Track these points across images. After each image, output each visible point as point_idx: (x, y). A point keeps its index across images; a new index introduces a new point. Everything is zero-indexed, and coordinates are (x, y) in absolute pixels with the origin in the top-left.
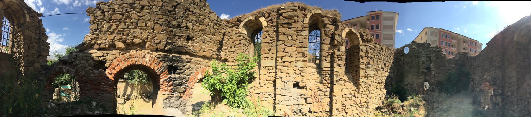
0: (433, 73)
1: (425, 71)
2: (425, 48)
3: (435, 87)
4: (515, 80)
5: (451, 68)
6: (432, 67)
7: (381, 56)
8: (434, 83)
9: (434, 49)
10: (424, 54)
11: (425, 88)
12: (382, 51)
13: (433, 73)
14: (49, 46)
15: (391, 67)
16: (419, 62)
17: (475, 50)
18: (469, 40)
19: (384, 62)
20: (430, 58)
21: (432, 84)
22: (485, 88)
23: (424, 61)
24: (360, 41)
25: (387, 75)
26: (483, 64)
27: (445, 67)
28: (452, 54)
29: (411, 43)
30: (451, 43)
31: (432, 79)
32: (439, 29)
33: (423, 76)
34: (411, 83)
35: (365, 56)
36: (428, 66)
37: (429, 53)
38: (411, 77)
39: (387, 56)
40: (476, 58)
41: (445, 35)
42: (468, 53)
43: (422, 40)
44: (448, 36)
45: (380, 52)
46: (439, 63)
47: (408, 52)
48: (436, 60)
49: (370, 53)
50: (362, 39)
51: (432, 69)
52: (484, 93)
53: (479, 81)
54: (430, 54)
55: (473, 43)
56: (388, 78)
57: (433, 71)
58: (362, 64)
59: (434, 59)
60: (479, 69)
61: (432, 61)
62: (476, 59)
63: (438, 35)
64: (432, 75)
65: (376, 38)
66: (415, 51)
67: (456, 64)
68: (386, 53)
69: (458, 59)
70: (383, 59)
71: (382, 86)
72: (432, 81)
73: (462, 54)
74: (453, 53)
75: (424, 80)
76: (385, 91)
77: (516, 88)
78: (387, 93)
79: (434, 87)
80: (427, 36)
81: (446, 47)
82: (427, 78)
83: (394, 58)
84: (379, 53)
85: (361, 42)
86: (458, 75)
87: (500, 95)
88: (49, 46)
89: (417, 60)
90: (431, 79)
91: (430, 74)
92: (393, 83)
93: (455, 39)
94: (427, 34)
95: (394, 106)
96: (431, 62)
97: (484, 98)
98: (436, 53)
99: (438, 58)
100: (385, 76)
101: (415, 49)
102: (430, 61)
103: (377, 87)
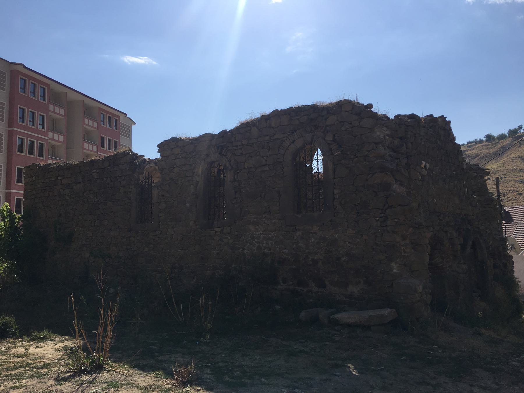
14: (452, 131)
17: (116, 142)
18: (100, 109)
32: (11, 63)
41: (29, 88)
44: (39, 92)
55: (109, 118)
81: (24, 128)
88: (452, 131)
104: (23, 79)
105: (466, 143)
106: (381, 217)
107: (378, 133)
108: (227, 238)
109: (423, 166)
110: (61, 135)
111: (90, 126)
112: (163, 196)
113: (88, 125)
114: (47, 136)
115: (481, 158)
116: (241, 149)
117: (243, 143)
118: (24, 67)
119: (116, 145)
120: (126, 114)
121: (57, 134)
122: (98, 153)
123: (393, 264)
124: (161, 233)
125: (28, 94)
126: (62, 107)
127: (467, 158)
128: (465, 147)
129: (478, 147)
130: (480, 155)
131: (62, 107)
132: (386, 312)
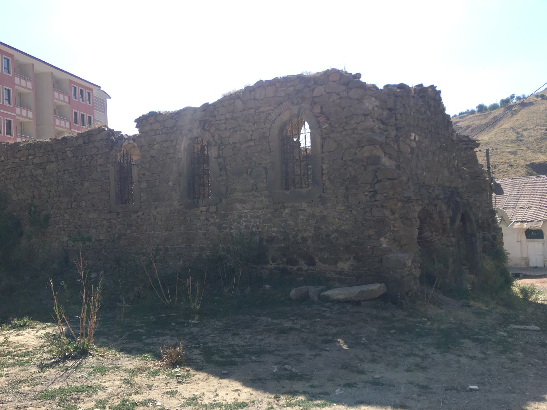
17: (90, 118)
18: (71, 82)
65: (7, 134)
105: (458, 114)
106: (370, 192)
107: (367, 105)
108: (214, 217)
109: (412, 138)
112: (144, 174)
113: (59, 99)
115: (473, 129)
116: (225, 123)
117: (227, 116)
120: (100, 87)
121: (26, 110)
122: (71, 130)
123: (382, 239)
124: (143, 214)
127: (459, 130)
128: (457, 118)
129: (470, 118)
130: (472, 126)
132: (375, 287)
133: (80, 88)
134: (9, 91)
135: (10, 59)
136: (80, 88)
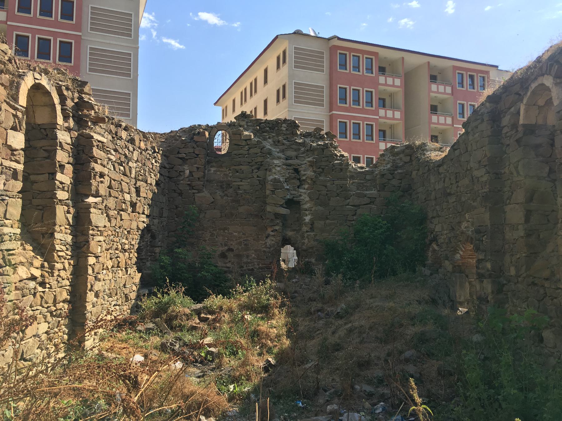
0: (307, 219)
1: (284, 211)
2: (280, 138)
3: (316, 260)
4: (522, 233)
5: (366, 200)
6: (305, 198)
7: (131, 164)
8: (312, 248)
9: (308, 140)
10: (279, 158)
11: (283, 265)
12: (131, 149)
13: (307, 219)
15: (152, 199)
16: (263, 182)
18: (455, 68)
19: (135, 184)
20: (297, 171)
21: (305, 251)
22: (470, 260)
23: (280, 182)
24: (58, 117)
25: (142, 226)
26: (458, 187)
27: (347, 198)
28: (384, 136)
29: (235, 118)
30: (376, 89)
31: (306, 235)
32: (329, 39)
33: (277, 228)
34: (238, 249)
35: (68, 163)
36: (292, 197)
37: (293, 154)
38: (239, 232)
39: (144, 165)
40: (439, 166)
42: (422, 148)
43: (266, 82)
44: (363, 64)
45: (127, 152)
46: (326, 186)
47: (227, 148)
48: (316, 177)
49: (99, 161)
50: (62, 109)
51: (306, 206)
52: (467, 276)
53: (450, 239)
54: (297, 157)
55: (472, 77)
56: (146, 233)
57: (307, 212)
58: (61, 186)
59: (310, 173)
60: (448, 202)
61: (304, 180)
62: (441, 170)
63: (326, 64)
64: (306, 224)
66: (250, 148)
67: (383, 187)
68: (141, 153)
69: (388, 170)
70: (133, 176)
71: (130, 259)
72: (306, 241)
73: (403, 152)
74: (388, 133)
75: (279, 238)
76: (138, 277)
77: (524, 255)
78: (144, 283)
79: (313, 260)
80: (285, 69)
81: (346, 110)
82: (290, 233)
83: (162, 167)
84: (126, 157)
85: (60, 120)
86: (385, 222)
87: (490, 276)
89: (258, 177)
90: (303, 237)
91: (300, 220)
92: (157, 250)
93: (394, 74)
94: (284, 62)
95: (173, 311)
96: (301, 183)
97: (468, 291)
98: (316, 153)
99: (323, 169)
100: (138, 228)
101: (249, 142)
102: (299, 179)
103: (119, 263)
104: (356, 56)
110: (397, 111)
111: (441, 93)
113: (437, 92)
114: (378, 115)
118: (339, 39)
119: (330, 91)
120: (497, 67)
125: (478, 89)
126: (396, 76)
131: (396, 76)
133: (469, 73)
134: (463, 105)
135: (464, 72)
136: (469, 73)
